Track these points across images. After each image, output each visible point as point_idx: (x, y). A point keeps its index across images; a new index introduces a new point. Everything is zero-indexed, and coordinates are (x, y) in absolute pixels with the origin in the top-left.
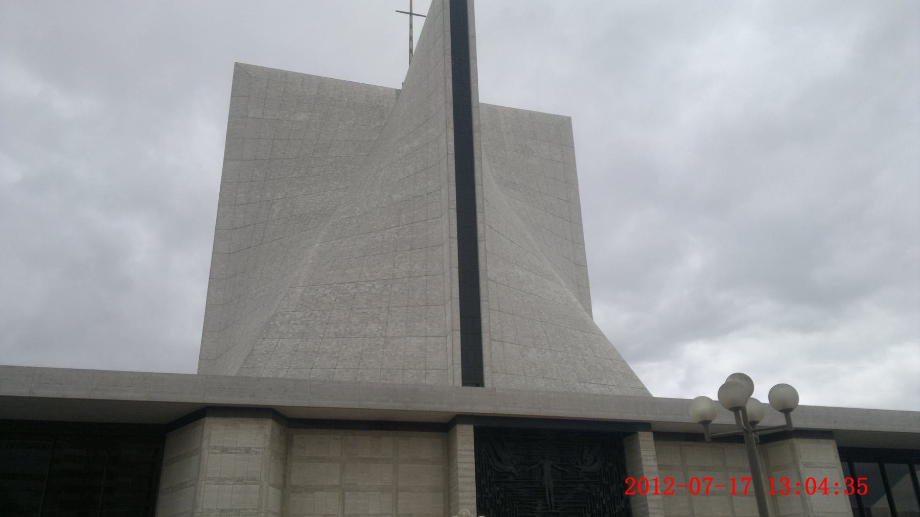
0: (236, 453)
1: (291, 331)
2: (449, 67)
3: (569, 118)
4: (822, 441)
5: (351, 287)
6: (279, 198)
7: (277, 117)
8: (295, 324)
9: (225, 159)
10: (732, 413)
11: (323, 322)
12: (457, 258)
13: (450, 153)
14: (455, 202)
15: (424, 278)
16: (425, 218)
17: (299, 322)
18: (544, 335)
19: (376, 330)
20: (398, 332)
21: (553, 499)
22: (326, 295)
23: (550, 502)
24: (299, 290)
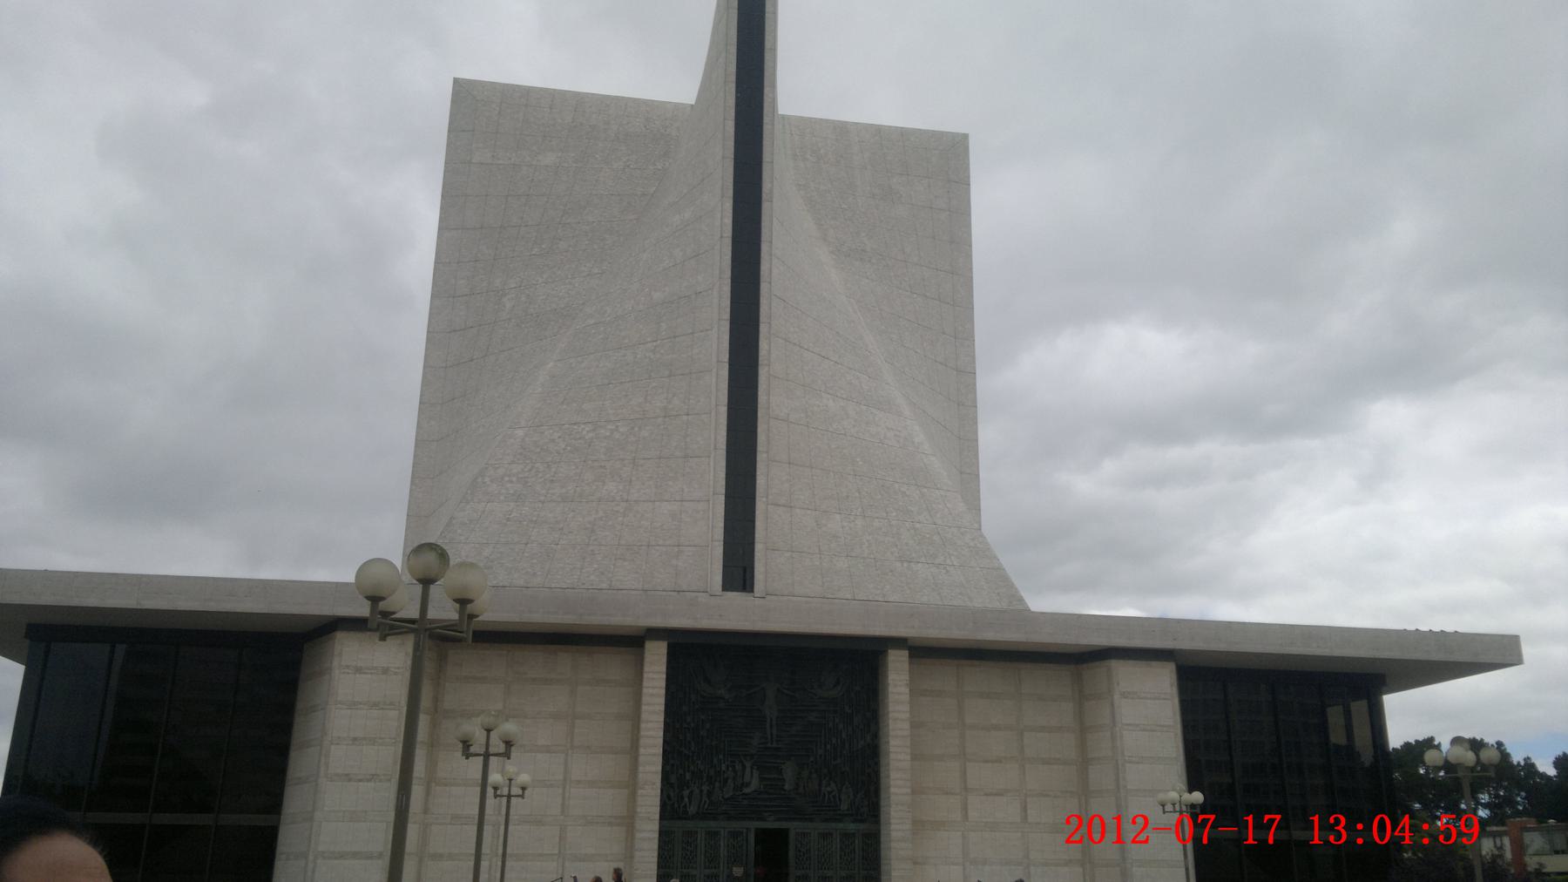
0: (371, 673)
1: (503, 491)
2: (732, 102)
3: (966, 136)
4: (1154, 663)
5: (587, 429)
6: (513, 286)
7: (513, 160)
8: (511, 482)
9: (440, 229)
10: (485, 732)
11: (545, 480)
12: (726, 392)
13: (725, 235)
14: (728, 310)
15: (685, 418)
16: (690, 331)
17: (514, 479)
18: (857, 494)
19: (615, 491)
20: (645, 493)
21: (775, 732)
22: (553, 441)
23: (772, 735)
24: (520, 433)
